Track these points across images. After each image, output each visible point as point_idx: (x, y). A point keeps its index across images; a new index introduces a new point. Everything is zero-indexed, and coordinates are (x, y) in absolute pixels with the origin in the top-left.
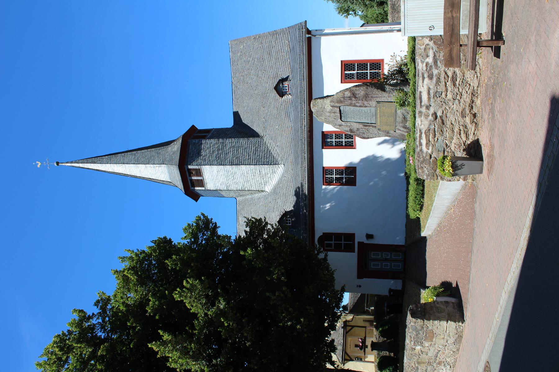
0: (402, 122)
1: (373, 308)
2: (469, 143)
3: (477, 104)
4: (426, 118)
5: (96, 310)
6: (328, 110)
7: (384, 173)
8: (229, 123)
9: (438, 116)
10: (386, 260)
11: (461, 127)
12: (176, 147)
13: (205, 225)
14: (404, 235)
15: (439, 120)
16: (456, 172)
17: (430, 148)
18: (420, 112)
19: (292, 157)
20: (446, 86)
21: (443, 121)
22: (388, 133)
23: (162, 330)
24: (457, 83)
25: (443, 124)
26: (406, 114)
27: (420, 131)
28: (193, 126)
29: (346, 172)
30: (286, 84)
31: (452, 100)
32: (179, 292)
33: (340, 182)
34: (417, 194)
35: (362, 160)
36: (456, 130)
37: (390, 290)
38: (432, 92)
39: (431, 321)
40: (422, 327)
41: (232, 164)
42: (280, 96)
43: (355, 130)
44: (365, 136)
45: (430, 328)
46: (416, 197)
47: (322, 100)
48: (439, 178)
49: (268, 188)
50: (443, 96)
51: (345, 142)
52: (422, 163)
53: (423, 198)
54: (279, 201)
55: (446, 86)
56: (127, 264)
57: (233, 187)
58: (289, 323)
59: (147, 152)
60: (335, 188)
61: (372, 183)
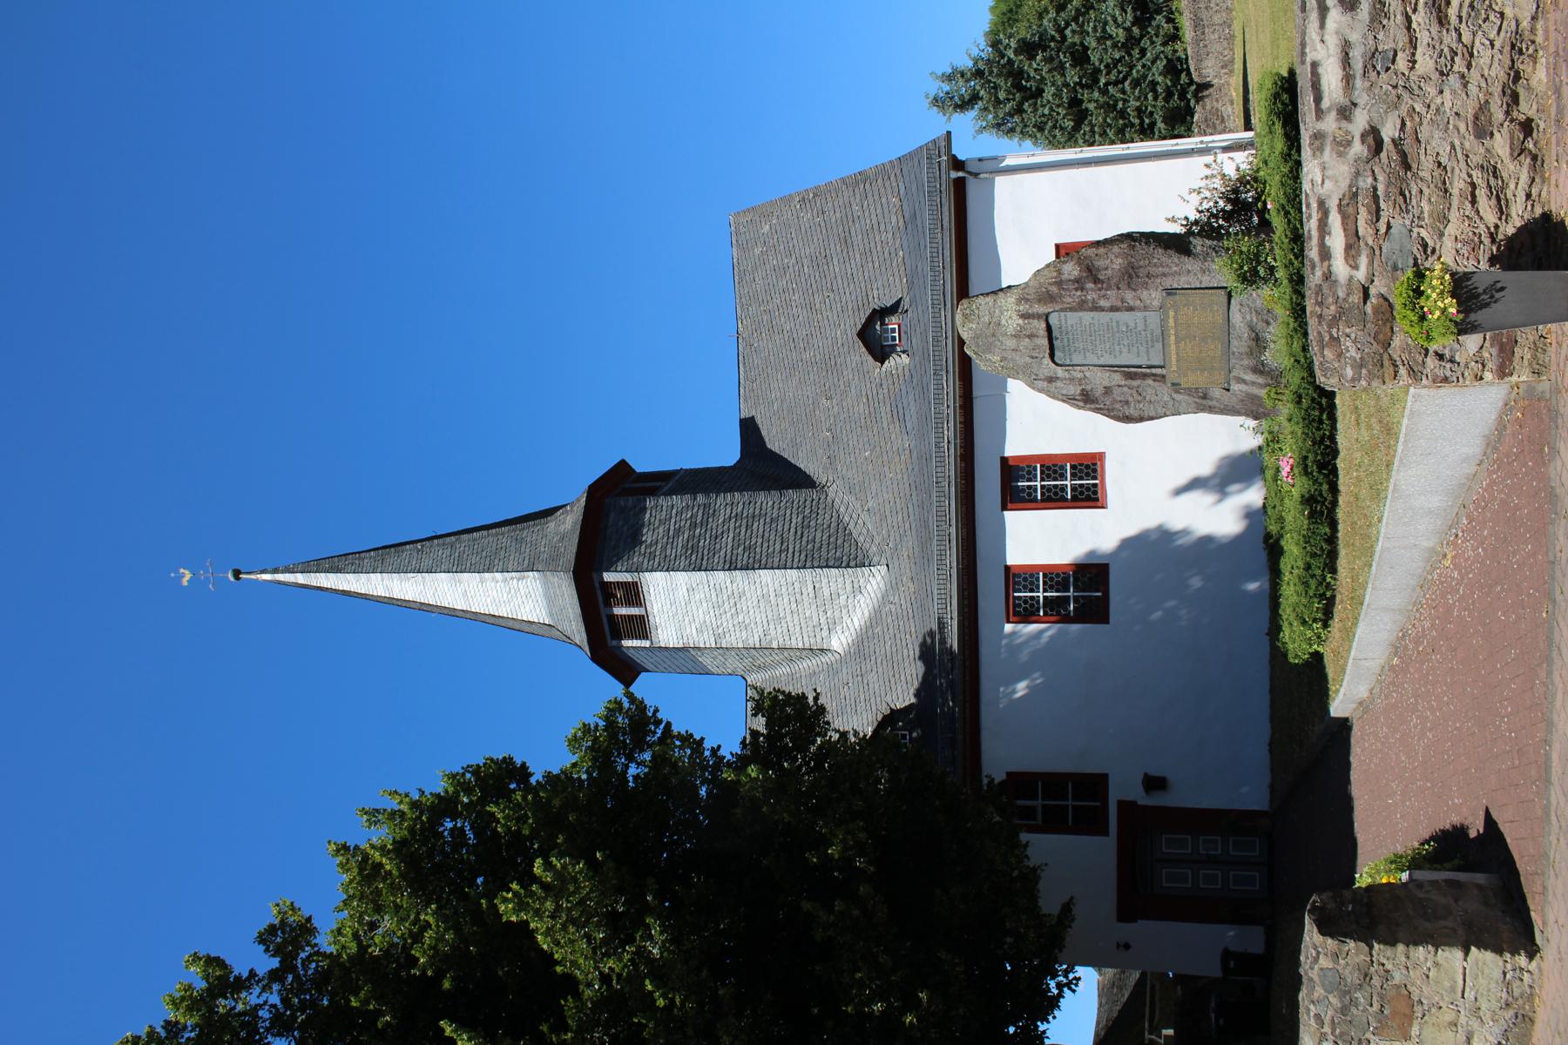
0: (1251, 353)
1: (1170, 1032)
2: (1510, 231)
3: (1534, 83)
4: (1340, 154)
5: (267, 963)
6: (1010, 330)
7: (1196, 582)
8: (727, 453)
9: (1386, 139)
11: (1476, 174)
12: (569, 523)
13: (633, 726)
14: (1267, 779)
15: (1392, 155)
16: (1473, 317)
17: (1363, 261)
18: (1318, 136)
19: (910, 542)
20: (1409, 28)
21: (1404, 156)
22: (1205, 397)
23: (452, 1021)
24: (1452, 12)
25: (1408, 167)
26: (1260, 326)
27: (1322, 204)
28: (623, 463)
29: (1076, 579)
30: (893, 323)
31: (1435, 76)
32: (516, 894)
33: (1058, 614)
34: (1314, 555)
35: (1128, 544)
36: (1458, 185)
37: (1227, 955)
38: (1357, 55)
39: (1401, 947)
40: (1366, 976)
41: (731, 566)
42: (876, 359)
43: (1099, 392)
44: (1131, 411)
45: (1398, 977)
46: (1308, 567)
47: (990, 299)
48: (1403, 371)
49: (839, 642)
50: (1402, 63)
51: (1074, 489)
52: (1334, 322)
53: (1334, 571)
54: (872, 677)
55: (1409, 28)
56: (382, 834)
57: (734, 639)
58: (878, 1007)
59: (488, 540)
60: (1042, 631)
61: (1158, 614)
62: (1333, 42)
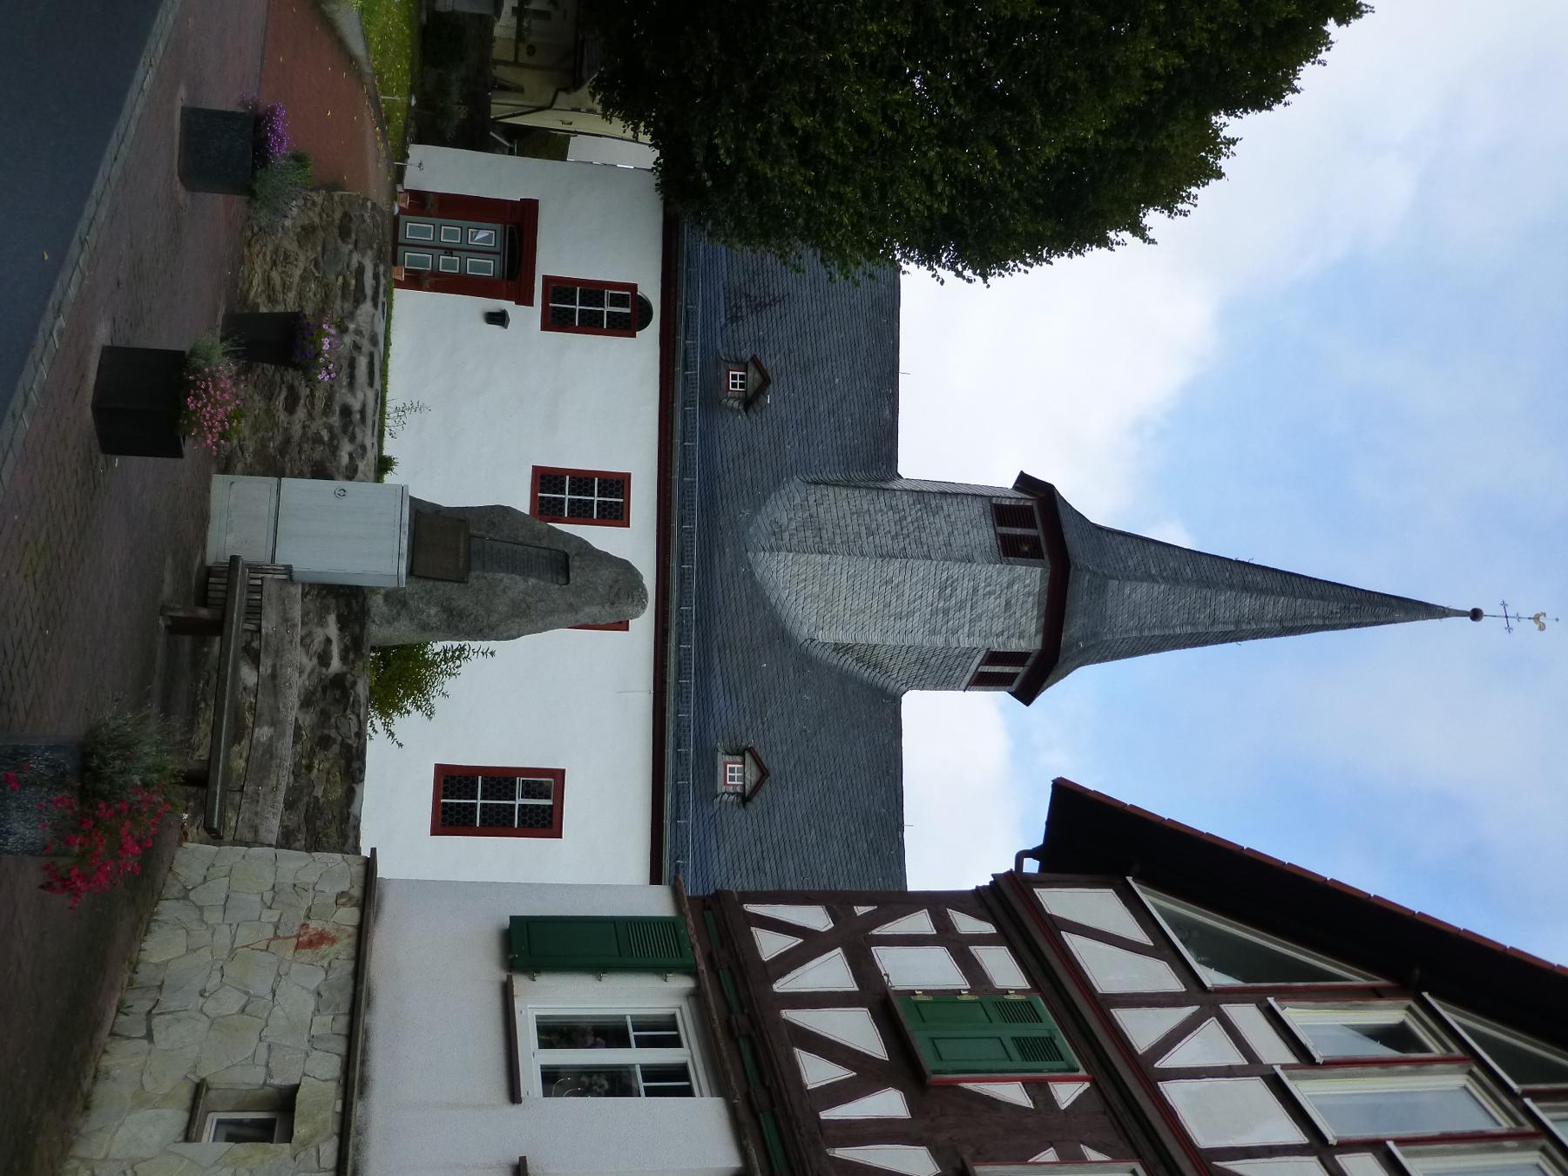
10: (449, 251)
62: (360, 395)
